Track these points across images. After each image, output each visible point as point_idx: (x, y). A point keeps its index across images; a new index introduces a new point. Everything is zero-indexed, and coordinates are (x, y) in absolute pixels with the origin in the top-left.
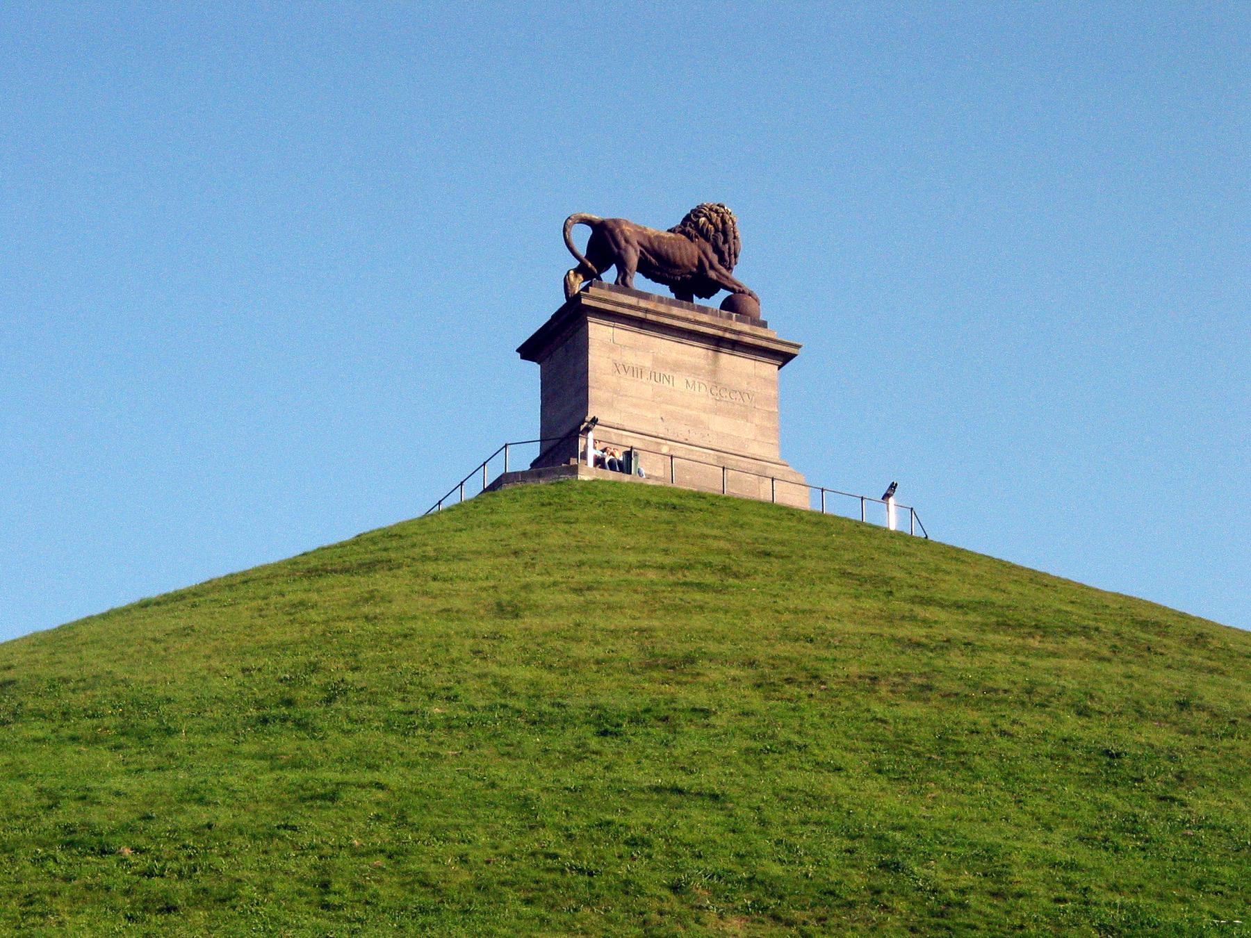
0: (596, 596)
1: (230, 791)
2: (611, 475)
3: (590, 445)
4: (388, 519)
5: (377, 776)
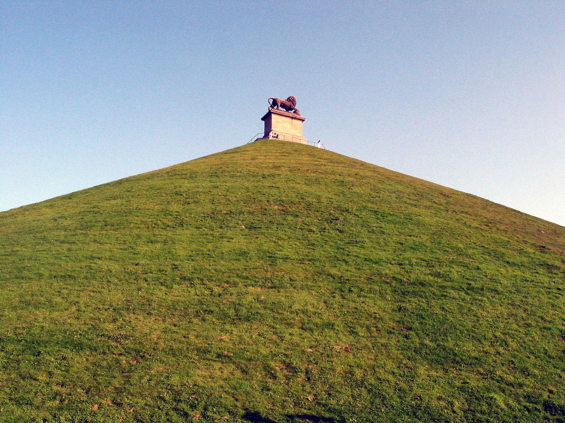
0: (267, 157)
1: (203, 186)
2: (275, 139)
3: (271, 134)
4: (239, 146)
5: (226, 184)
